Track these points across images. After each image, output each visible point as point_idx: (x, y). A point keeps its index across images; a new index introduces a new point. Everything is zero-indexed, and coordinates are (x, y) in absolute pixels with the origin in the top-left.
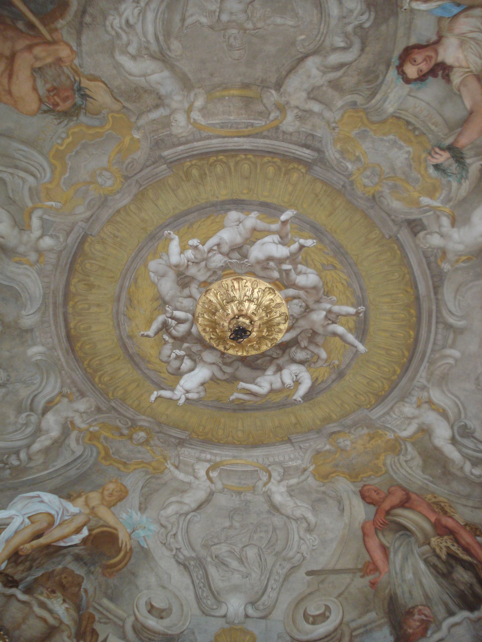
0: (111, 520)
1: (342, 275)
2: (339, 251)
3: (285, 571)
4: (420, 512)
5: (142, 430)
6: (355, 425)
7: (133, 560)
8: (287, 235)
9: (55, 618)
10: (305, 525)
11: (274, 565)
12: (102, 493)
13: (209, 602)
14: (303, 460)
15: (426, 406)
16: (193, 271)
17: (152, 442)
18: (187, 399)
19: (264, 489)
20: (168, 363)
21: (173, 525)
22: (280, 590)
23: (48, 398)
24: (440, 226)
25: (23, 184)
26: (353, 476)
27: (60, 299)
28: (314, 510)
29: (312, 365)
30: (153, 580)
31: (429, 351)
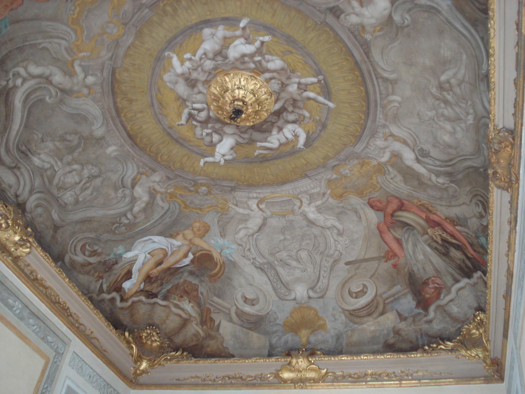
0: (205, 246)
1: (298, 57)
2: (290, 40)
3: (330, 264)
4: (413, 213)
5: (204, 186)
6: (347, 159)
7: (226, 270)
8: (249, 36)
9: (186, 314)
10: (336, 231)
11: (321, 262)
12: (193, 230)
13: (282, 291)
14: (320, 188)
15: (390, 139)
16: (194, 75)
17: (212, 192)
18: (225, 160)
19: (300, 211)
20: (203, 139)
21: (246, 243)
22: (329, 277)
23: (132, 177)
24: (353, 8)
25: (60, 46)
26: (360, 194)
27: (114, 114)
28: (339, 220)
29: (302, 123)
30: (243, 281)
31: (379, 99)
